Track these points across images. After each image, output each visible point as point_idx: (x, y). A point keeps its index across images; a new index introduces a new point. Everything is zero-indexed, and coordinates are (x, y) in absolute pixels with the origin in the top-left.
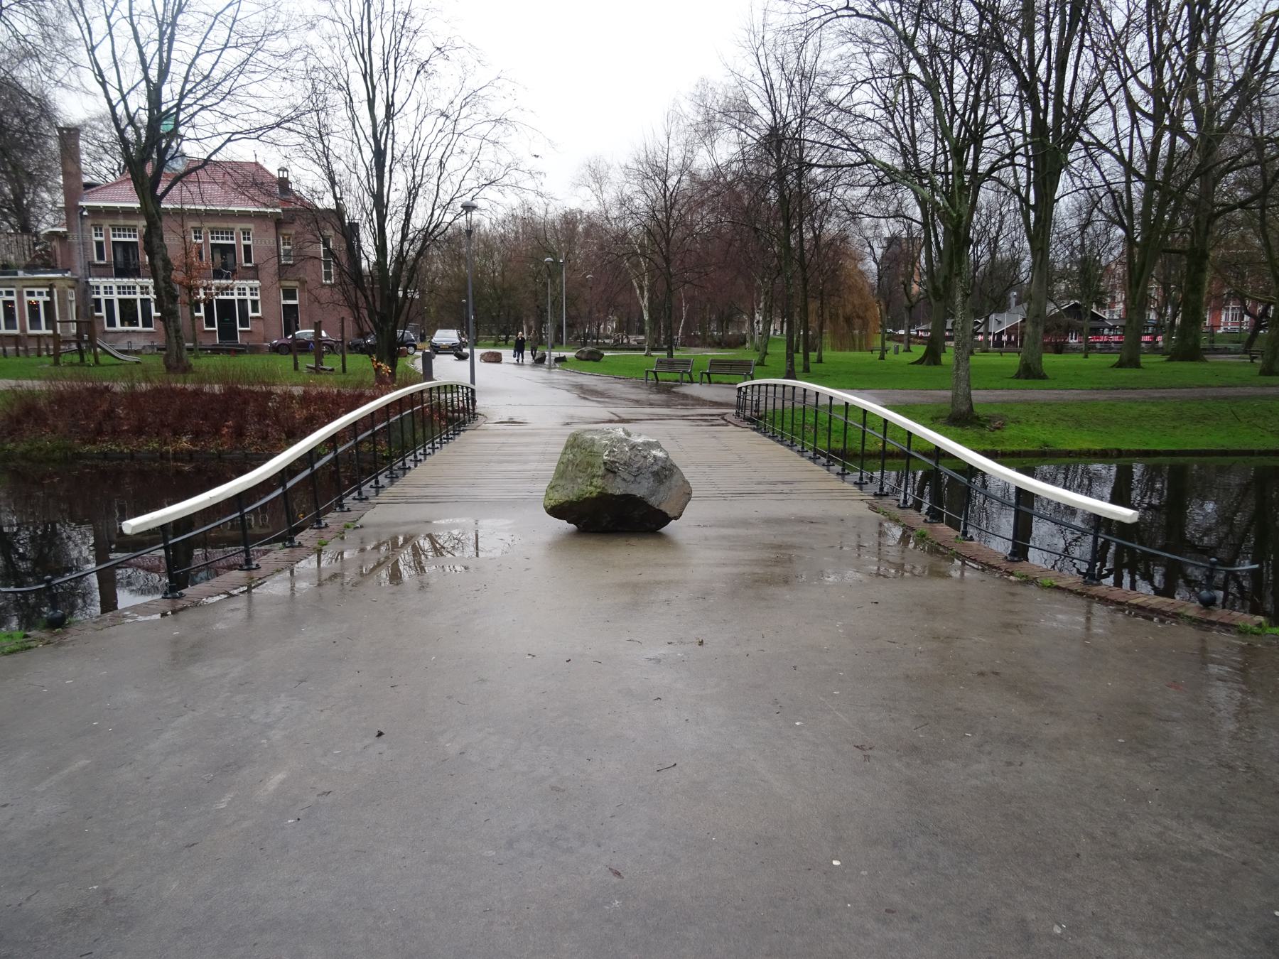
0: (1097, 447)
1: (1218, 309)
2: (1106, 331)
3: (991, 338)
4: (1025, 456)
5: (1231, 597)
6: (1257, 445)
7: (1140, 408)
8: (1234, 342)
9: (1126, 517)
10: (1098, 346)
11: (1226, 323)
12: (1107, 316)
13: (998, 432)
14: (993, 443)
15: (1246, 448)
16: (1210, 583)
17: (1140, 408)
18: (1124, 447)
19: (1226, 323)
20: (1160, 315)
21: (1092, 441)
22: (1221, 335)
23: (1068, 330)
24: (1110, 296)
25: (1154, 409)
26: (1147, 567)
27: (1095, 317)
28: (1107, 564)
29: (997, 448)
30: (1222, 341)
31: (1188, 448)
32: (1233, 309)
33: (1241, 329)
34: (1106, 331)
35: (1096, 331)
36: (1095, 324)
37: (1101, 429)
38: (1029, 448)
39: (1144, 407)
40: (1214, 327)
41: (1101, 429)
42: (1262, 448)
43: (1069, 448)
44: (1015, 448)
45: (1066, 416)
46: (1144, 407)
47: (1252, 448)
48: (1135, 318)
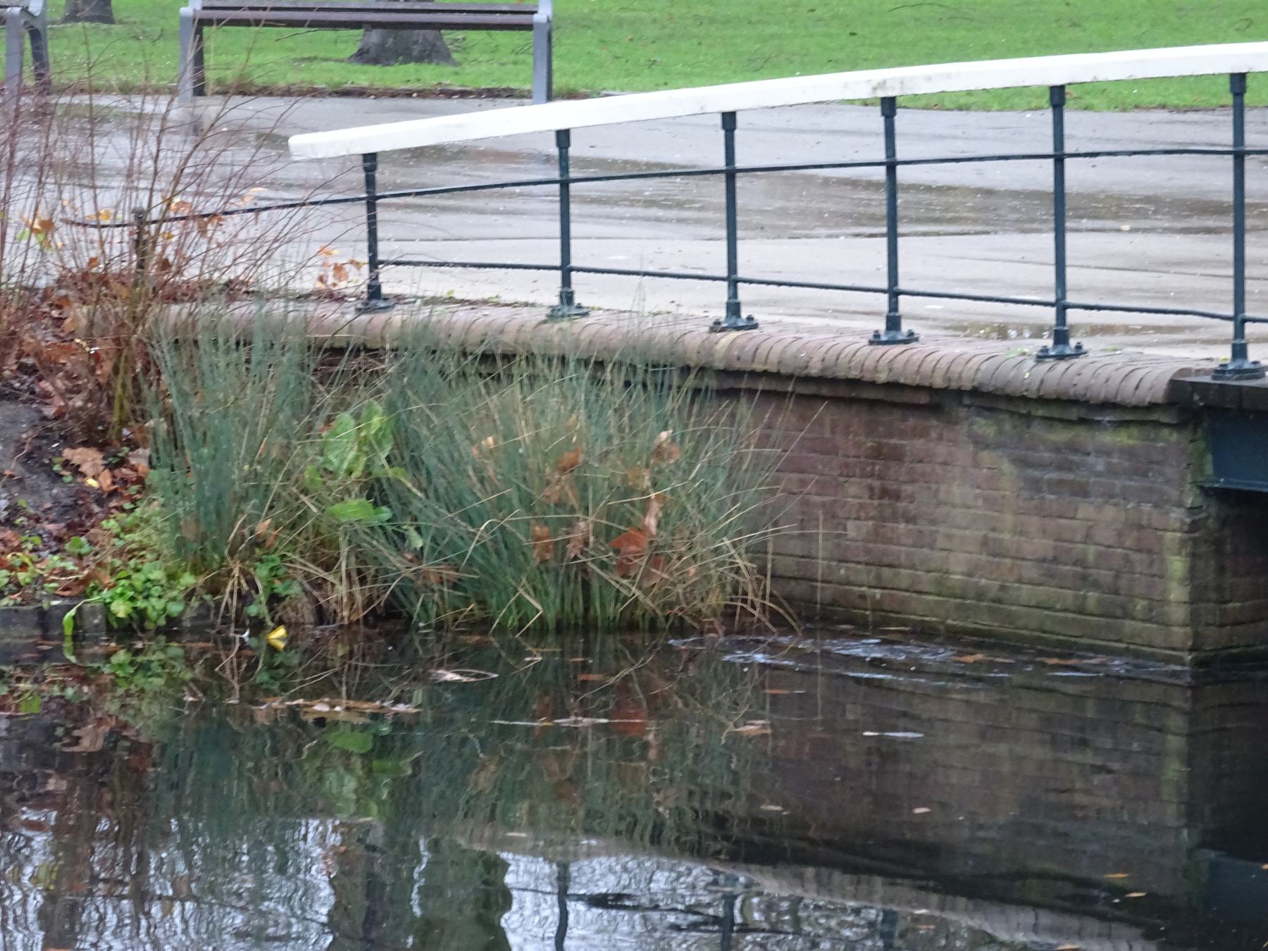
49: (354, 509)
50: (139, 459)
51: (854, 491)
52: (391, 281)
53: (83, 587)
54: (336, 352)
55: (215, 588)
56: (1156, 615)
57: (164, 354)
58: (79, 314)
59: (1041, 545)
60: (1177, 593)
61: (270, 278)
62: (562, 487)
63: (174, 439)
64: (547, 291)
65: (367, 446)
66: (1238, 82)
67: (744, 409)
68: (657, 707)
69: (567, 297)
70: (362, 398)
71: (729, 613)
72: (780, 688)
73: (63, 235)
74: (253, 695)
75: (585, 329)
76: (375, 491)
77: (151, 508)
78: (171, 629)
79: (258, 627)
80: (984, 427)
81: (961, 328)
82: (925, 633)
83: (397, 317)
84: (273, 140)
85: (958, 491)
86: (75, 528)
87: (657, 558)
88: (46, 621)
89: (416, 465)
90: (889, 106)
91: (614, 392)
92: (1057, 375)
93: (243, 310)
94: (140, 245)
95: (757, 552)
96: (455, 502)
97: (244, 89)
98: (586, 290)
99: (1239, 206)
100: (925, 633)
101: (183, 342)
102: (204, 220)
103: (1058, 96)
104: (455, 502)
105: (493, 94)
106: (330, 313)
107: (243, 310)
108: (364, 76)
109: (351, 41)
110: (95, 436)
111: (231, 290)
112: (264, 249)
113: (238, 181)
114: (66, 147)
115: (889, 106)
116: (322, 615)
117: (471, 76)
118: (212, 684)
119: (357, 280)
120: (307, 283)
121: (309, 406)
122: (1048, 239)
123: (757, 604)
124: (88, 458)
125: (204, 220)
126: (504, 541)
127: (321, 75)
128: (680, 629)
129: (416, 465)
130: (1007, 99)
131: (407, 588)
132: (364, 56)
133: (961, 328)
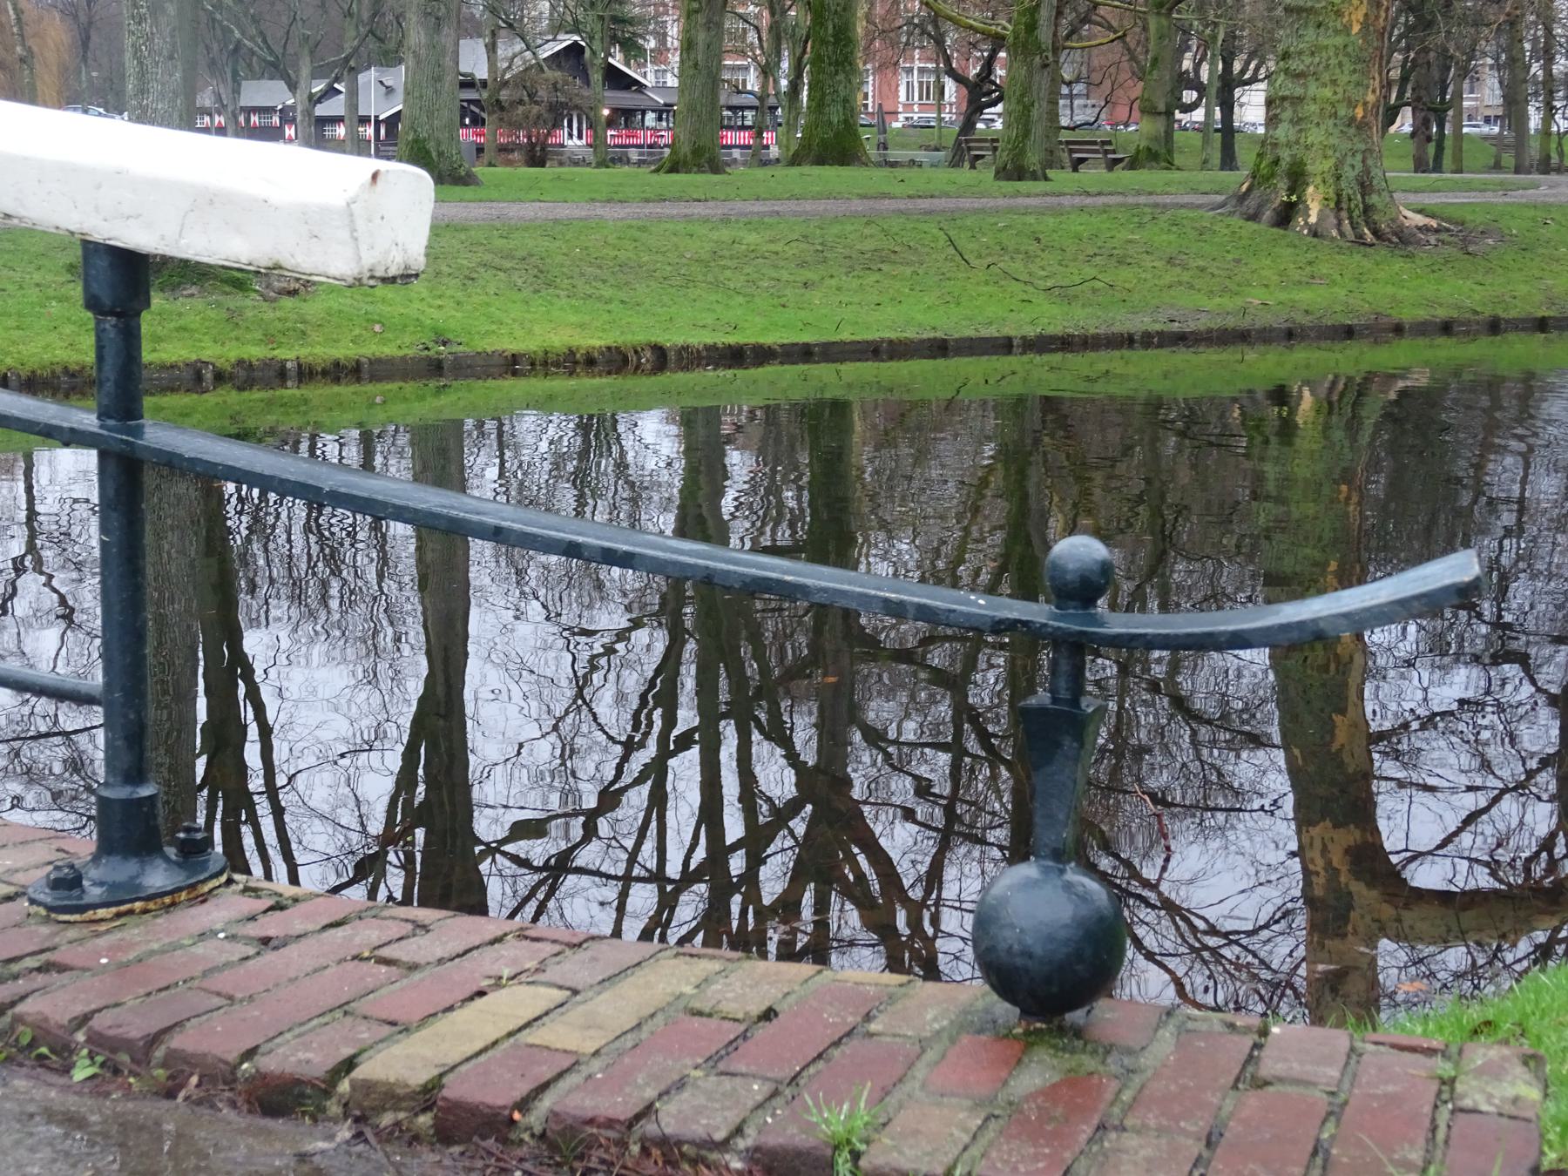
0: (595, 341)
1: (889, 67)
2: (650, 118)
3: (370, 131)
4: (375, 378)
5: (967, 760)
6: (1020, 325)
7: (715, 235)
8: (928, 148)
9: (312, 221)
10: (634, 155)
11: (908, 107)
12: (649, 81)
13: (288, 302)
14: (269, 339)
15: (991, 332)
16: (643, 606)
17: (715, 235)
18: (672, 338)
19: (908, 107)
20: (767, 71)
21: (582, 326)
22: (899, 132)
23: (558, 114)
24: (655, 33)
25: (752, 238)
26: (775, 715)
27: (617, 79)
28: (682, 714)
29: (281, 353)
30: (903, 146)
31: (845, 336)
32: (922, 71)
33: (940, 119)
34: (650, 118)
35: (625, 117)
36: (626, 99)
37: (607, 292)
38: (388, 351)
39: (725, 234)
40: (884, 115)
41: (607, 292)
42: (1031, 332)
43: (512, 347)
44: (344, 351)
45: (509, 256)
46: (725, 234)
47: (1008, 331)
48: (701, 37)
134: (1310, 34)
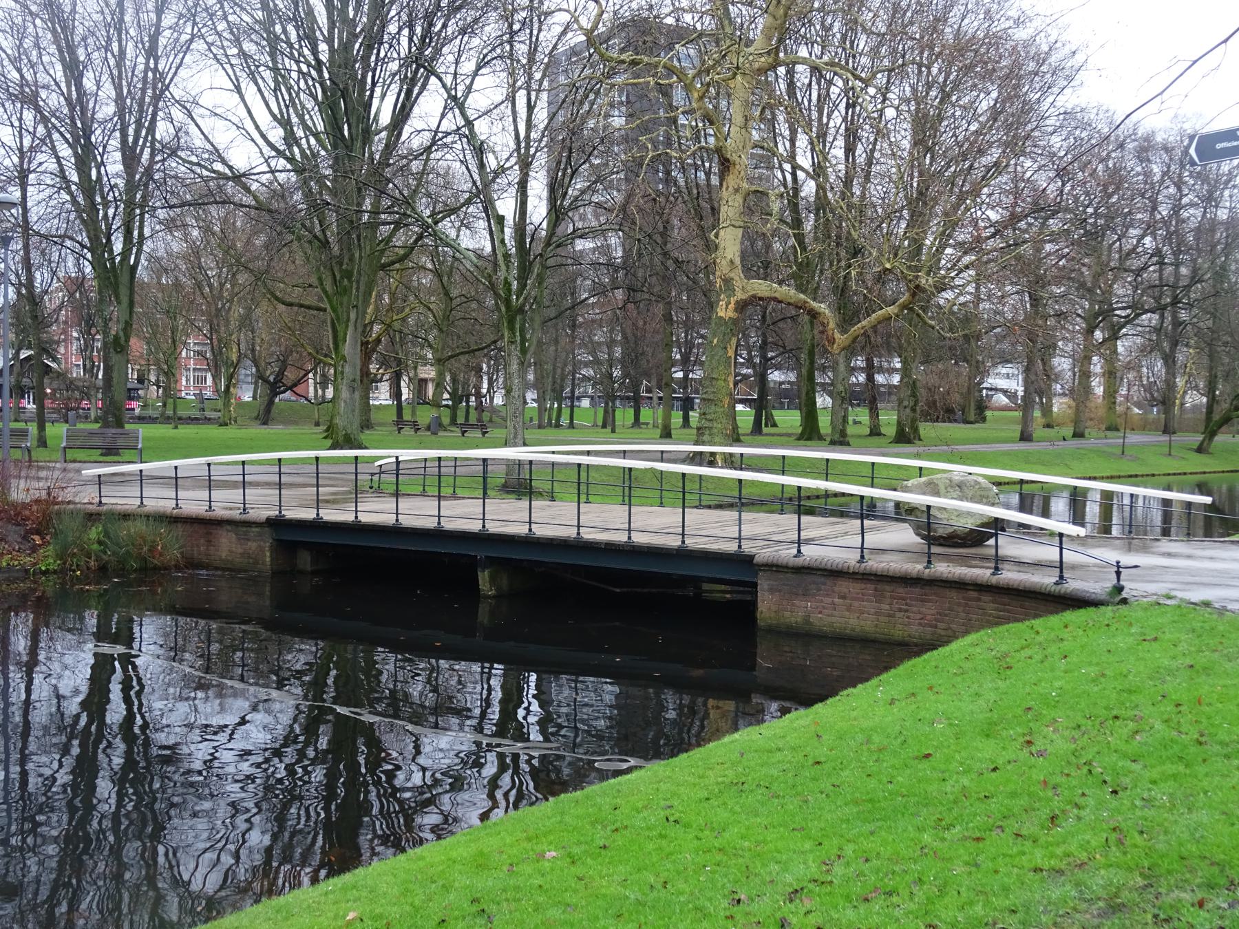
49: (95, 547)
50: (48, 537)
51: (202, 541)
52: (104, 500)
53: (35, 564)
54: (91, 515)
55: (64, 563)
56: (264, 563)
57: (53, 516)
58: (35, 508)
59: (240, 551)
60: (268, 559)
61: (77, 500)
62: (140, 541)
63: (56, 534)
64: (138, 502)
65: (98, 534)
66: (280, 460)
67: (179, 525)
68: (161, 584)
69: (799, 551)
70: (97, 524)
71: (175, 566)
72: (714, 444)
73: (31, 492)
74: (73, 585)
75: (145, 510)
76: (100, 543)
77: (51, 547)
78: (55, 572)
79: (74, 571)
80: (229, 528)
81: (226, 508)
82: (217, 569)
83: (105, 508)
84: (79, 471)
85: (224, 540)
86: (34, 552)
87: (161, 555)
88: (27, 571)
89: (109, 538)
90: (209, 465)
91: (151, 522)
92: (244, 517)
93: (71, 506)
94: (49, 494)
95: (182, 553)
96: (117, 544)
97: (74, 461)
98: (146, 502)
99: (280, 484)
100: (217, 569)
101: (58, 513)
102: (63, 488)
103: (243, 463)
104: (117, 544)
105: (129, 462)
106: (90, 507)
107: (71, 506)
108: (101, 459)
109: (99, 451)
110: (38, 533)
111: (69, 503)
112: (76, 495)
113: (70, 480)
114: (33, 473)
115: (209, 465)
116: (88, 568)
117: (125, 458)
118: (63, 584)
119: (97, 500)
120: (86, 501)
121: (85, 526)
122: (241, 491)
123: (182, 563)
124: (37, 538)
125: (63, 488)
126: (128, 552)
127: (92, 459)
128: (166, 569)
129: (109, 538)
130: (235, 463)
131: (107, 562)
132: (102, 455)
133: (226, 508)
134: (713, 407)
